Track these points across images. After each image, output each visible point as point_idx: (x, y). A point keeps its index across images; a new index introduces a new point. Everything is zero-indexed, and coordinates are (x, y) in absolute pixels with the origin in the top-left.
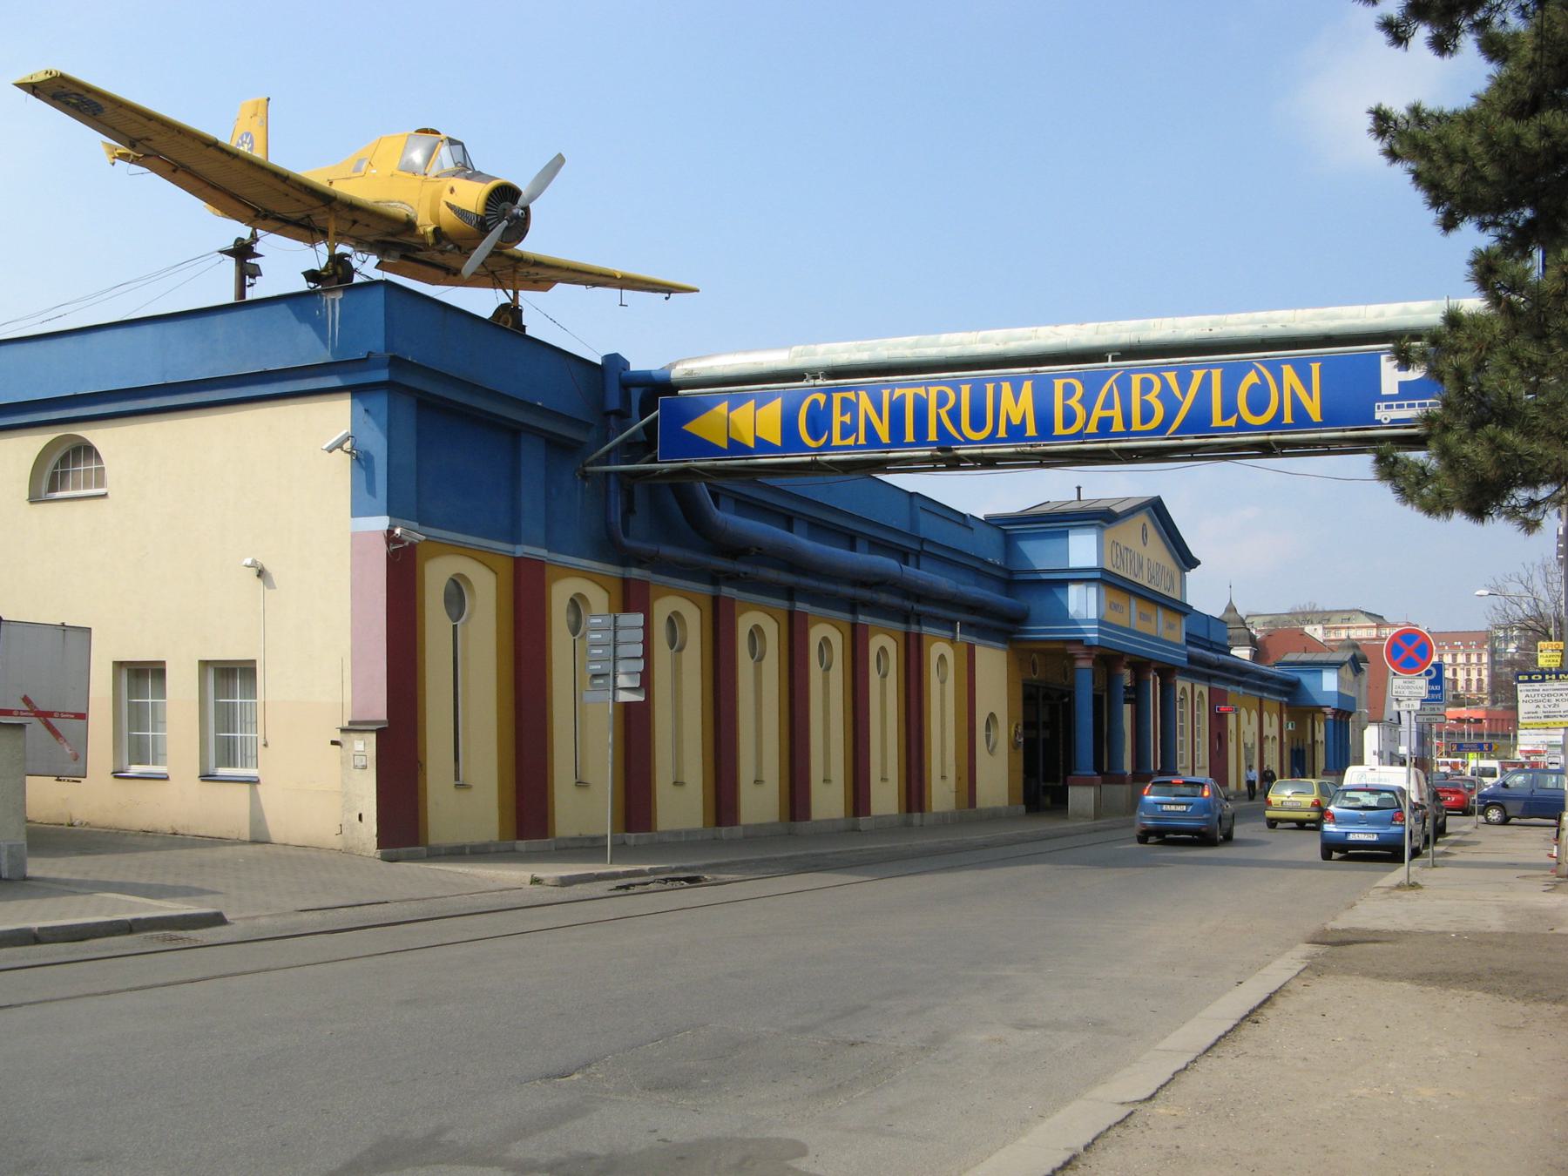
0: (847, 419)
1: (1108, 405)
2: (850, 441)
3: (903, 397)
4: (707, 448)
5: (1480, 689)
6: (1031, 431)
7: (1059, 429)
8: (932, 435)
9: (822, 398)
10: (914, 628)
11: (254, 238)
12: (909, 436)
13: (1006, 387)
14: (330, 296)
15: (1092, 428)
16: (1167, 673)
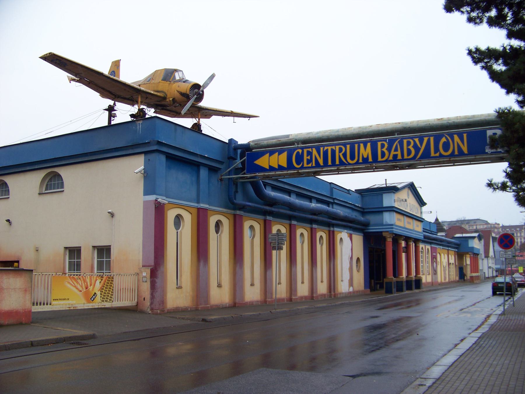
0: (309, 158)
1: (396, 150)
2: (310, 165)
3: (327, 150)
6: (370, 160)
7: (380, 159)
8: (337, 162)
9: (300, 151)
10: (332, 229)
11: (114, 104)
12: (330, 163)
13: (362, 145)
14: (139, 122)
15: (391, 158)
16: (416, 241)
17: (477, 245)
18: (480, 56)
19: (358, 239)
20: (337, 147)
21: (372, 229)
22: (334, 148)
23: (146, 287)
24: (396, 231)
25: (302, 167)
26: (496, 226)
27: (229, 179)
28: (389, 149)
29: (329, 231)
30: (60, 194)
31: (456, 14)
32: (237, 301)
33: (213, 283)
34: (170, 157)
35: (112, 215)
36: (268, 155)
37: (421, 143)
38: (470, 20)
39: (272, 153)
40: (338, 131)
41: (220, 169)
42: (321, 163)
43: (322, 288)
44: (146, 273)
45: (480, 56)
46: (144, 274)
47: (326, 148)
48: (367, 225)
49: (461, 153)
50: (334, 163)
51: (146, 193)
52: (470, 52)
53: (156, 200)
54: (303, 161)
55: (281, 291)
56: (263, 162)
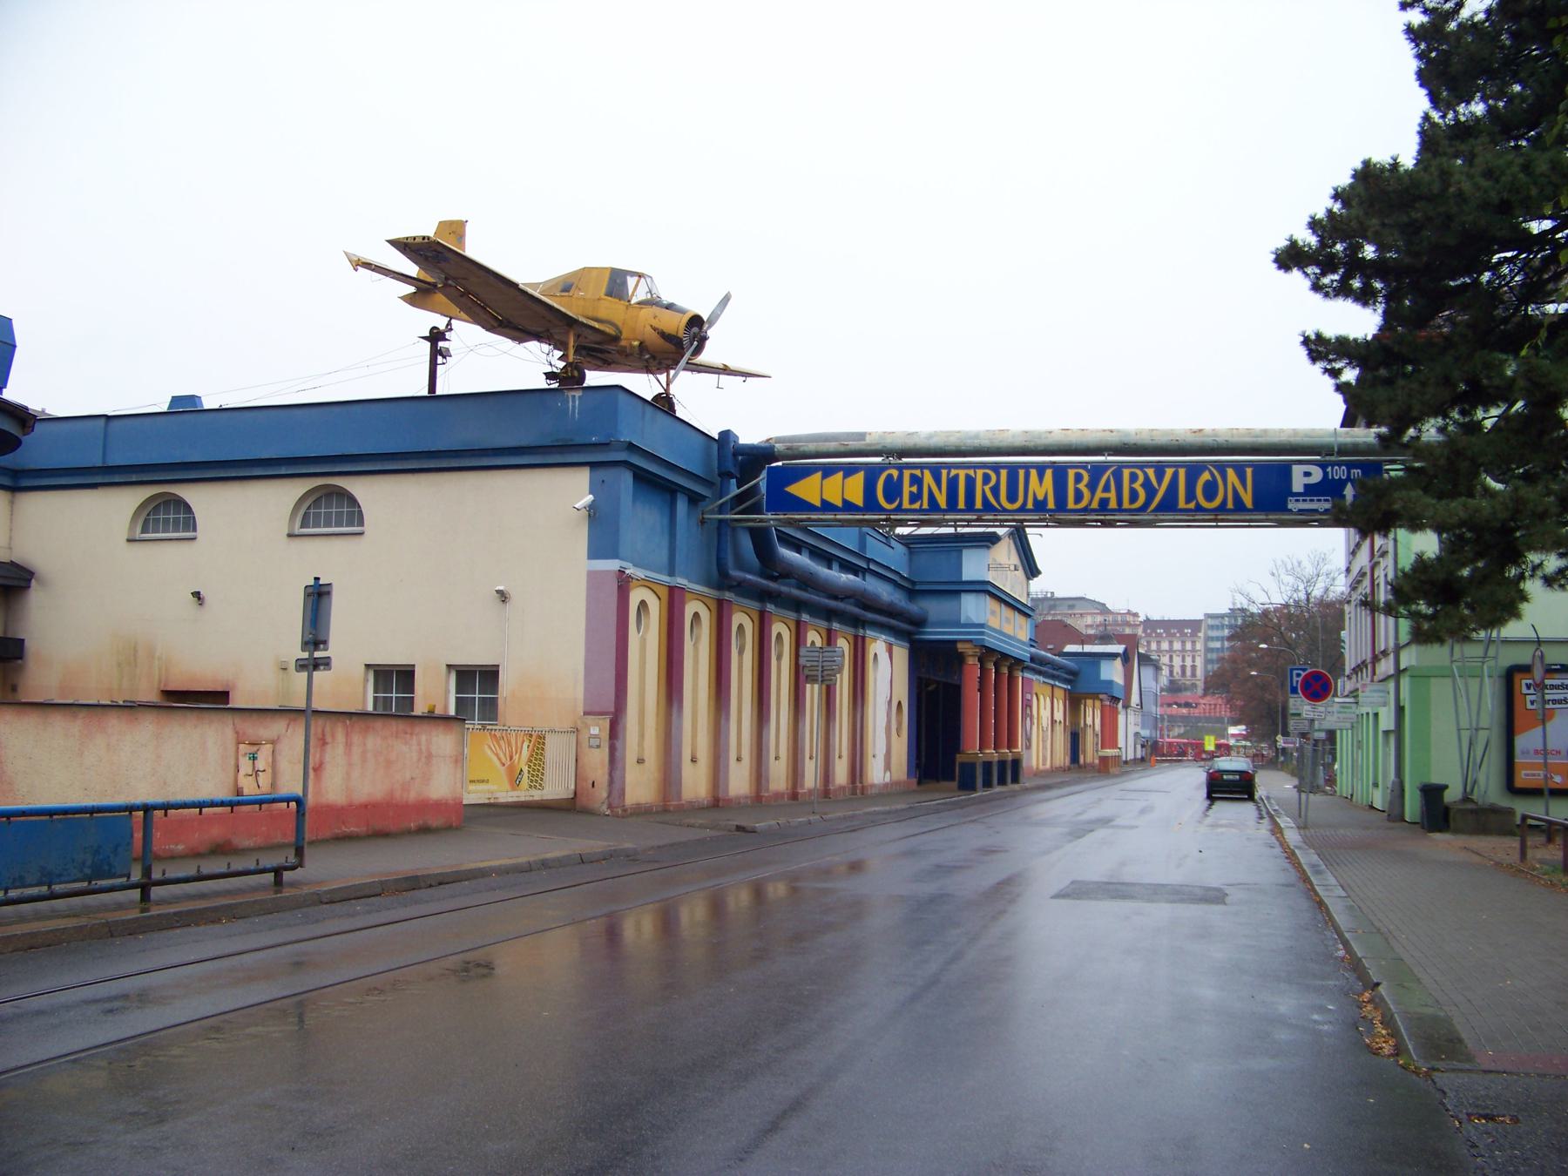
0: (914, 489)
1: (1106, 489)
2: (916, 506)
3: (957, 476)
4: (809, 507)
5: (1194, 674)
6: (1051, 505)
7: (1071, 505)
8: (979, 504)
9: (895, 473)
10: (861, 632)
11: (449, 328)
12: (961, 505)
13: (1033, 473)
14: (571, 393)
15: (1095, 505)
16: (1017, 663)
17: (1113, 672)
18: (1319, 348)
19: (901, 653)
20: (980, 473)
21: (933, 633)
22: (971, 472)
23: (597, 760)
24: (991, 641)
25: (899, 509)
26: (1130, 619)
27: (720, 521)
28: (1092, 487)
29: (856, 637)
30: (356, 539)
31: (1296, 274)
32: (721, 795)
33: (733, 755)
34: (643, 479)
35: (503, 596)
36: (819, 475)
37: (1160, 481)
38: (1316, 287)
39: (828, 471)
40: (977, 436)
41: (703, 498)
42: (943, 505)
43: (811, 778)
44: (598, 728)
45: (1319, 348)
46: (595, 731)
47: (953, 472)
48: (920, 622)
49: (1239, 506)
50: (970, 506)
51: (595, 552)
52: (1306, 342)
53: (621, 572)
54: (900, 494)
55: (695, 783)
56: (807, 489)
